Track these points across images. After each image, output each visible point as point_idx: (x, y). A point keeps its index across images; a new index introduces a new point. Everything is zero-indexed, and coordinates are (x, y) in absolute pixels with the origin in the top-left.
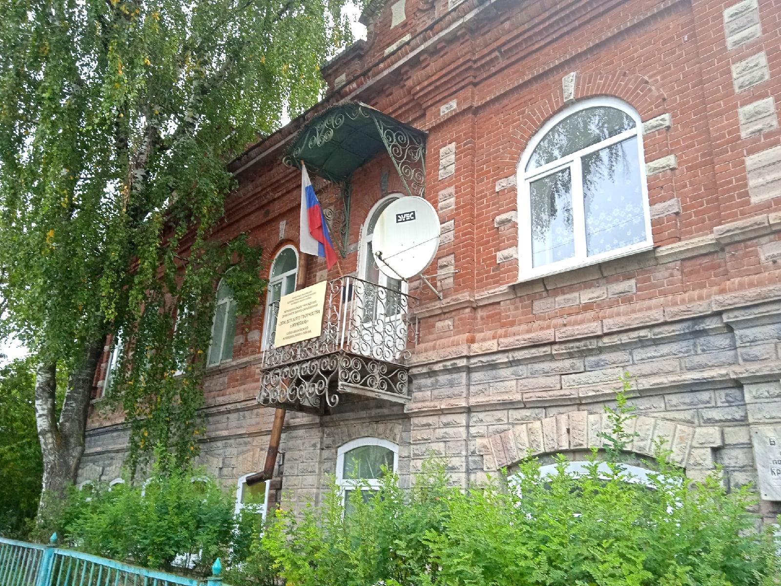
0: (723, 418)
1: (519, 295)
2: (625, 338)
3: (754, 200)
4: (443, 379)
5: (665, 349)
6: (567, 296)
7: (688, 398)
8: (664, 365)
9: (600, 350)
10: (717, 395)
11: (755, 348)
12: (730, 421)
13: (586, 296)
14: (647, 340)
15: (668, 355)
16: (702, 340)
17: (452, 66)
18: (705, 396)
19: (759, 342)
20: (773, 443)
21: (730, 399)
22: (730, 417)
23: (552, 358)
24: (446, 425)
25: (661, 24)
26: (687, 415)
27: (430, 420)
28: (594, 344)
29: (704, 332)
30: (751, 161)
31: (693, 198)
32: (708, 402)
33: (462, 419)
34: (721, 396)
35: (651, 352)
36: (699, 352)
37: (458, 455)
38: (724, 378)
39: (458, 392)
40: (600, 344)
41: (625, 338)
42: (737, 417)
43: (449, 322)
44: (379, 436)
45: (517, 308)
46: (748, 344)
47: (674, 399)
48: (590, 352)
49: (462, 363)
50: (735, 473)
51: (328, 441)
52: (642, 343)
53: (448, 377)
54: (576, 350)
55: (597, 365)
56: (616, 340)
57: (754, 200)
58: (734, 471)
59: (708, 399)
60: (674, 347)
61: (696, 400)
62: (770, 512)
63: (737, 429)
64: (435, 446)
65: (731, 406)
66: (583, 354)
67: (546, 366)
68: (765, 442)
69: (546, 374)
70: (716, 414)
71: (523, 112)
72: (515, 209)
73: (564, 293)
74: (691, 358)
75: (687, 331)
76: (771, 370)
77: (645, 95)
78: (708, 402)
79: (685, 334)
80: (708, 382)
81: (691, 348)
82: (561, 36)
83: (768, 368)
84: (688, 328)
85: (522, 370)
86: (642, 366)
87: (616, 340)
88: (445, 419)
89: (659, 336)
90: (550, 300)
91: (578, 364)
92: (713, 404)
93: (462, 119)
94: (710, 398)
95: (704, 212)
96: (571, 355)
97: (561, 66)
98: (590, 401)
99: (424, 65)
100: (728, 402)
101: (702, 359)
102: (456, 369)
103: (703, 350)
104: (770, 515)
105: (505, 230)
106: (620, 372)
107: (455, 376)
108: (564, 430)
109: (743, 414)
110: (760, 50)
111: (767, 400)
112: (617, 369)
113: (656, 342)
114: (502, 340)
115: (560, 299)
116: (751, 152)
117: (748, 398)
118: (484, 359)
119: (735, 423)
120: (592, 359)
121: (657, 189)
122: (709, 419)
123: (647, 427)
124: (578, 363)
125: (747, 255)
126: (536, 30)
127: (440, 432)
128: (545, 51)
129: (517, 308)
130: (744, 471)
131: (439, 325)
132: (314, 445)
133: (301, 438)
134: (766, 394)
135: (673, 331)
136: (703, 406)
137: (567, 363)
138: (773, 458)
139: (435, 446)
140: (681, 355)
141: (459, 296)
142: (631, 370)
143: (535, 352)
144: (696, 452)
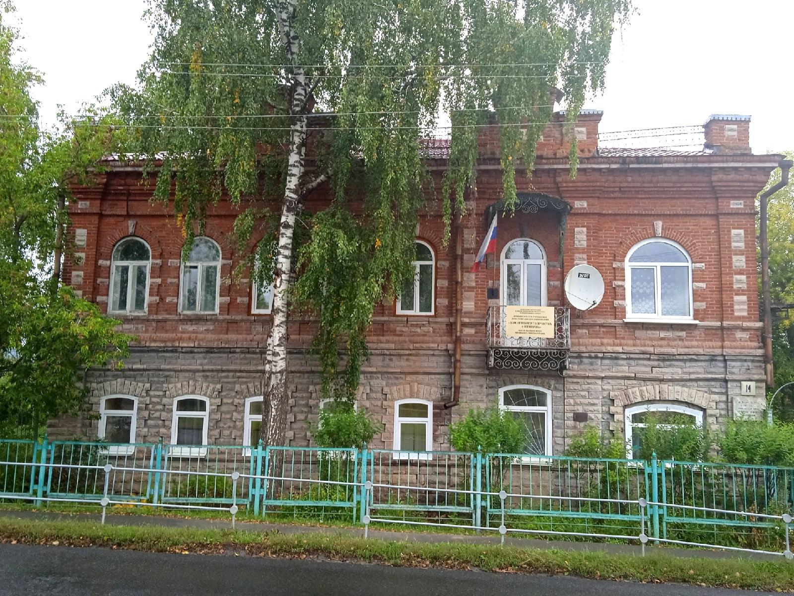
2: (685, 357)
3: (736, 314)
4: (585, 360)
5: (699, 364)
6: (653, 332)
7: (706, 383)
8: (698, 370)
9: (673, 360)
13: (663, 334)
16: (714, 363)
17: (725, 184)
18: (713, 383)
23: (649, 359)
24: (589, 384)
25: (702, 219)
26: (706, 389)
27: (579, 380)
28: (672, 357)
29: (716, 360)
31: (710, 304)
33: (599, 382)
34: (718, 384)
35: (693, 364)
37: (598, 398)
39: (602, 368)
41: (685, 357)
43: (584, 331)
44: (537, 384)
45: (625, 331)
47: (701, 383)
48: (668, 360)
49: (600, 355)
51: (494, 384)
52: (691, 360)
53: (590, 360)
55: (670, 366)
56: (681, 357)
57: (736, 314)
60: (703, 364)
64: (583, 393)
66: (664, 360)
67: (645, 362)
69: (645, 366)
70: (716, 390)
71: (629, 228)
72: (624, 280)
73: (651, 330)
77: (695, 251)
82: (654, 198)
85: (632, 362)
87: (681, 357)
88: (589, 381)
90: (645, 332)
93: (637, 217)
95: (714, 311)
96: (658, 360)
97: (658, 215)
99: (753, 174)
101: (712, 370)
102: (596, 357)
105: (619, 290)
106: (680, 371)
107: (595, 360)
108: (658, 391)
110: (743, 255)
113: (696, 361)
114: (625, 348)
115: (649, 332)
116: (736, 295)
117: (729, 386)
118: (613, 355)
120: (668, 363)
121: (697, 296)
124: (661, 364)
125: (731, 334)
126: (722, 188)
127: (586, 387)
128: (643, 201)
129: (625, 331)
131: (580, 331)
132: (481, 386)
133: (467, 380)
137: (656, 363)
139: (583, 393)
141: (597, 320)
142: (685, 370)
143: (642, 356)
144: (711, 403)
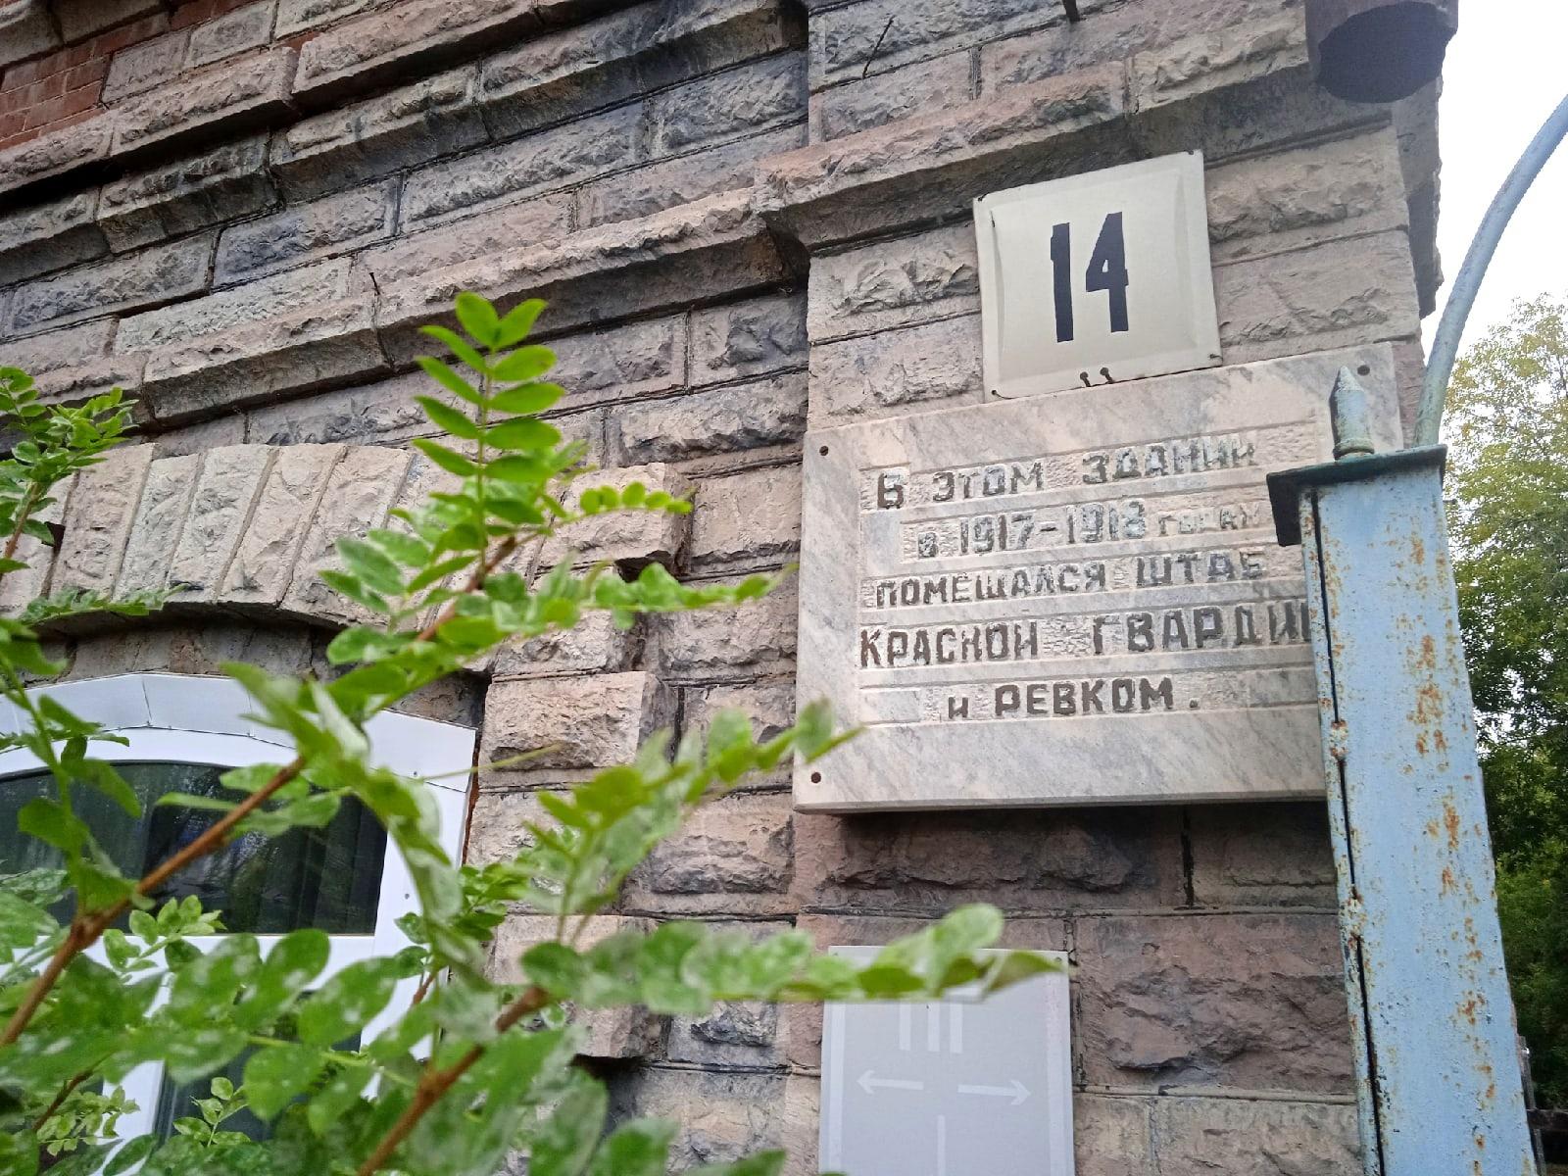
0: (704, 436)
1: (69, 35)
2: (375, 119)
10: (698, 332)
11: (884, 83)
12: (733, 444)
14: (462, 116)
15: (532, 178)
19: (906, 56)
20: (889, 496)
21: (750, 346)
22: (731, 428)
30: (933, 1043)
32: (656, 369)
36: (659, 149)
38: (732, 237)
40: (278, 158)
42: (768, 423)
46: (857, 71)
50: (715, 696)
52: (447, 136)
54: (184, 190)
55: (260, 258)
56: (337, 130)
58: (709, 684)
59: (655, 353)
61: (606, 364)
62: (831, 881)
63: (755, 479)
65: (747, 379)
68: (855, 497)
74: (620, 182)
75: (619, 53)
76: (939, 149)
78: (656, 369)
79: (611, 68)
80: (667, 264)
81: (632, 135)
83: (928, 142)
84: (625, 39)
86: (430, 238)
89: (509, 91)
91: (188, 261)
92: (676, 377)
94: (666, 348)
98: (186, 406)
100: (737, 358)
103: (676, 142)
104: (830, 899)
109: (791, 407)
111: (897, 317)
112: (328, 267)
119: (752, 456)
122: (646, 444)
123: (369, 488)
124: (191, 258)
130: (754, 681)
134: (903, 283)
135: (566, 58)
136: (629, 390)
138: (879, 572)
140: (588, 172)
